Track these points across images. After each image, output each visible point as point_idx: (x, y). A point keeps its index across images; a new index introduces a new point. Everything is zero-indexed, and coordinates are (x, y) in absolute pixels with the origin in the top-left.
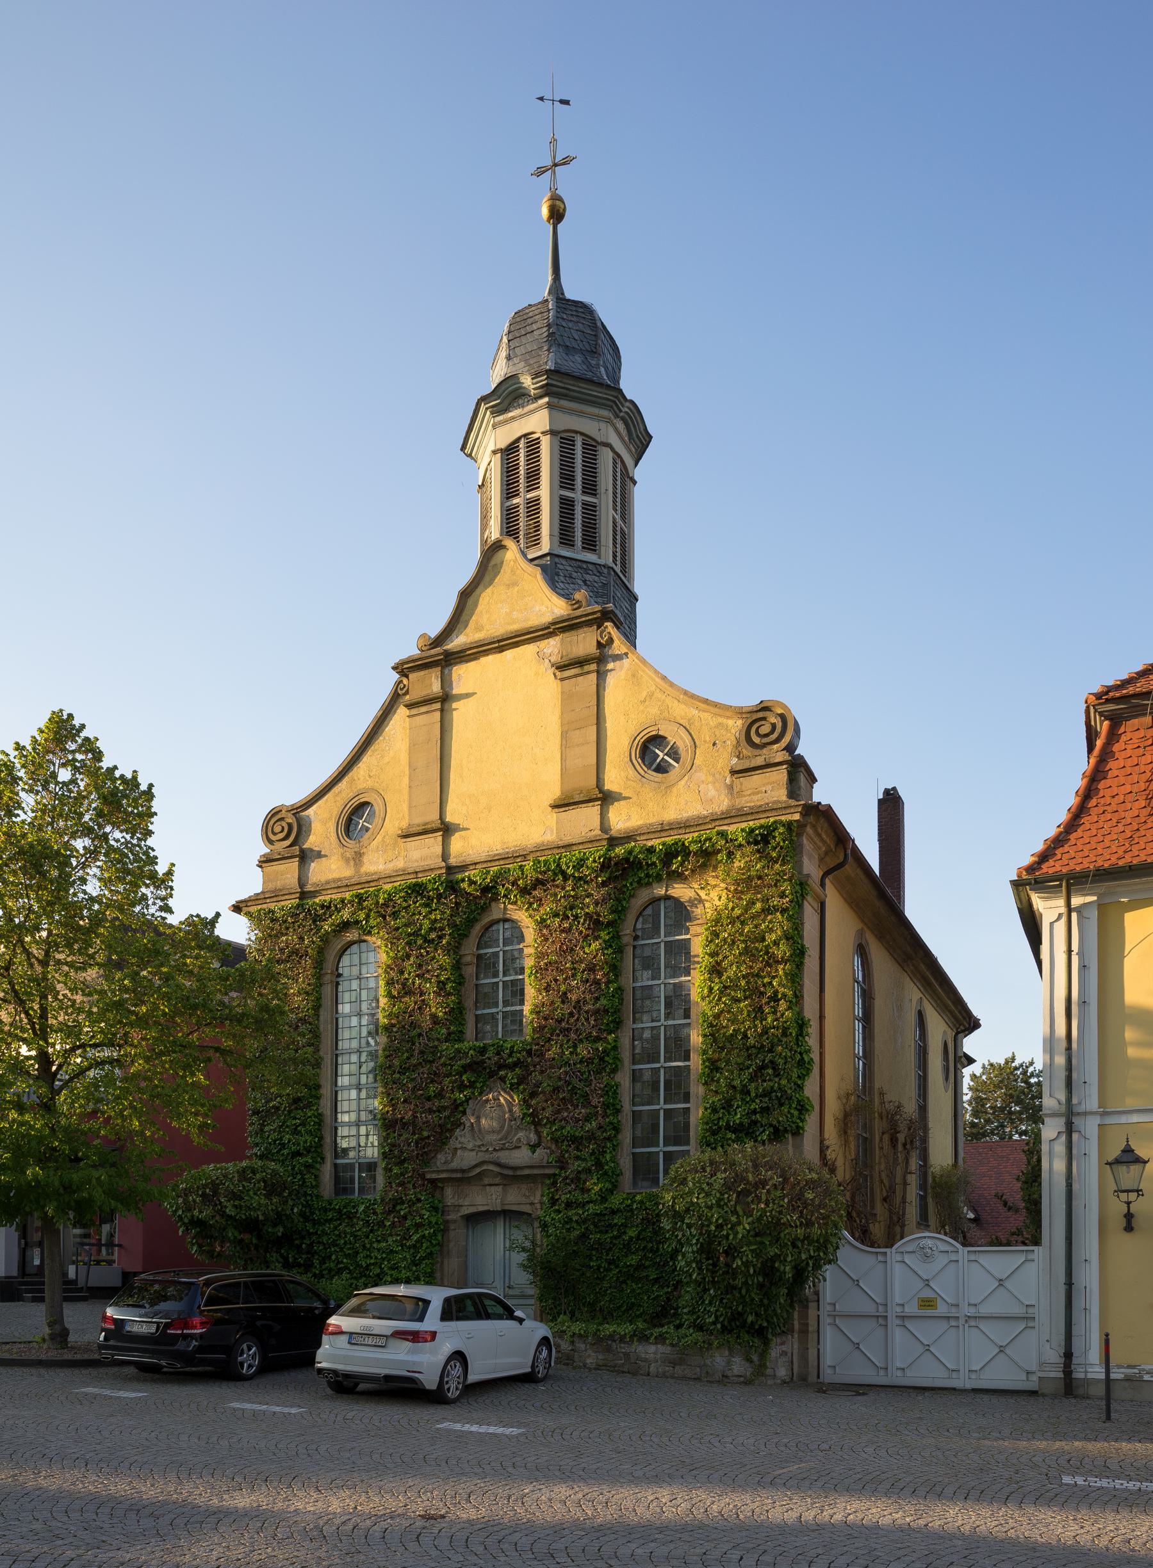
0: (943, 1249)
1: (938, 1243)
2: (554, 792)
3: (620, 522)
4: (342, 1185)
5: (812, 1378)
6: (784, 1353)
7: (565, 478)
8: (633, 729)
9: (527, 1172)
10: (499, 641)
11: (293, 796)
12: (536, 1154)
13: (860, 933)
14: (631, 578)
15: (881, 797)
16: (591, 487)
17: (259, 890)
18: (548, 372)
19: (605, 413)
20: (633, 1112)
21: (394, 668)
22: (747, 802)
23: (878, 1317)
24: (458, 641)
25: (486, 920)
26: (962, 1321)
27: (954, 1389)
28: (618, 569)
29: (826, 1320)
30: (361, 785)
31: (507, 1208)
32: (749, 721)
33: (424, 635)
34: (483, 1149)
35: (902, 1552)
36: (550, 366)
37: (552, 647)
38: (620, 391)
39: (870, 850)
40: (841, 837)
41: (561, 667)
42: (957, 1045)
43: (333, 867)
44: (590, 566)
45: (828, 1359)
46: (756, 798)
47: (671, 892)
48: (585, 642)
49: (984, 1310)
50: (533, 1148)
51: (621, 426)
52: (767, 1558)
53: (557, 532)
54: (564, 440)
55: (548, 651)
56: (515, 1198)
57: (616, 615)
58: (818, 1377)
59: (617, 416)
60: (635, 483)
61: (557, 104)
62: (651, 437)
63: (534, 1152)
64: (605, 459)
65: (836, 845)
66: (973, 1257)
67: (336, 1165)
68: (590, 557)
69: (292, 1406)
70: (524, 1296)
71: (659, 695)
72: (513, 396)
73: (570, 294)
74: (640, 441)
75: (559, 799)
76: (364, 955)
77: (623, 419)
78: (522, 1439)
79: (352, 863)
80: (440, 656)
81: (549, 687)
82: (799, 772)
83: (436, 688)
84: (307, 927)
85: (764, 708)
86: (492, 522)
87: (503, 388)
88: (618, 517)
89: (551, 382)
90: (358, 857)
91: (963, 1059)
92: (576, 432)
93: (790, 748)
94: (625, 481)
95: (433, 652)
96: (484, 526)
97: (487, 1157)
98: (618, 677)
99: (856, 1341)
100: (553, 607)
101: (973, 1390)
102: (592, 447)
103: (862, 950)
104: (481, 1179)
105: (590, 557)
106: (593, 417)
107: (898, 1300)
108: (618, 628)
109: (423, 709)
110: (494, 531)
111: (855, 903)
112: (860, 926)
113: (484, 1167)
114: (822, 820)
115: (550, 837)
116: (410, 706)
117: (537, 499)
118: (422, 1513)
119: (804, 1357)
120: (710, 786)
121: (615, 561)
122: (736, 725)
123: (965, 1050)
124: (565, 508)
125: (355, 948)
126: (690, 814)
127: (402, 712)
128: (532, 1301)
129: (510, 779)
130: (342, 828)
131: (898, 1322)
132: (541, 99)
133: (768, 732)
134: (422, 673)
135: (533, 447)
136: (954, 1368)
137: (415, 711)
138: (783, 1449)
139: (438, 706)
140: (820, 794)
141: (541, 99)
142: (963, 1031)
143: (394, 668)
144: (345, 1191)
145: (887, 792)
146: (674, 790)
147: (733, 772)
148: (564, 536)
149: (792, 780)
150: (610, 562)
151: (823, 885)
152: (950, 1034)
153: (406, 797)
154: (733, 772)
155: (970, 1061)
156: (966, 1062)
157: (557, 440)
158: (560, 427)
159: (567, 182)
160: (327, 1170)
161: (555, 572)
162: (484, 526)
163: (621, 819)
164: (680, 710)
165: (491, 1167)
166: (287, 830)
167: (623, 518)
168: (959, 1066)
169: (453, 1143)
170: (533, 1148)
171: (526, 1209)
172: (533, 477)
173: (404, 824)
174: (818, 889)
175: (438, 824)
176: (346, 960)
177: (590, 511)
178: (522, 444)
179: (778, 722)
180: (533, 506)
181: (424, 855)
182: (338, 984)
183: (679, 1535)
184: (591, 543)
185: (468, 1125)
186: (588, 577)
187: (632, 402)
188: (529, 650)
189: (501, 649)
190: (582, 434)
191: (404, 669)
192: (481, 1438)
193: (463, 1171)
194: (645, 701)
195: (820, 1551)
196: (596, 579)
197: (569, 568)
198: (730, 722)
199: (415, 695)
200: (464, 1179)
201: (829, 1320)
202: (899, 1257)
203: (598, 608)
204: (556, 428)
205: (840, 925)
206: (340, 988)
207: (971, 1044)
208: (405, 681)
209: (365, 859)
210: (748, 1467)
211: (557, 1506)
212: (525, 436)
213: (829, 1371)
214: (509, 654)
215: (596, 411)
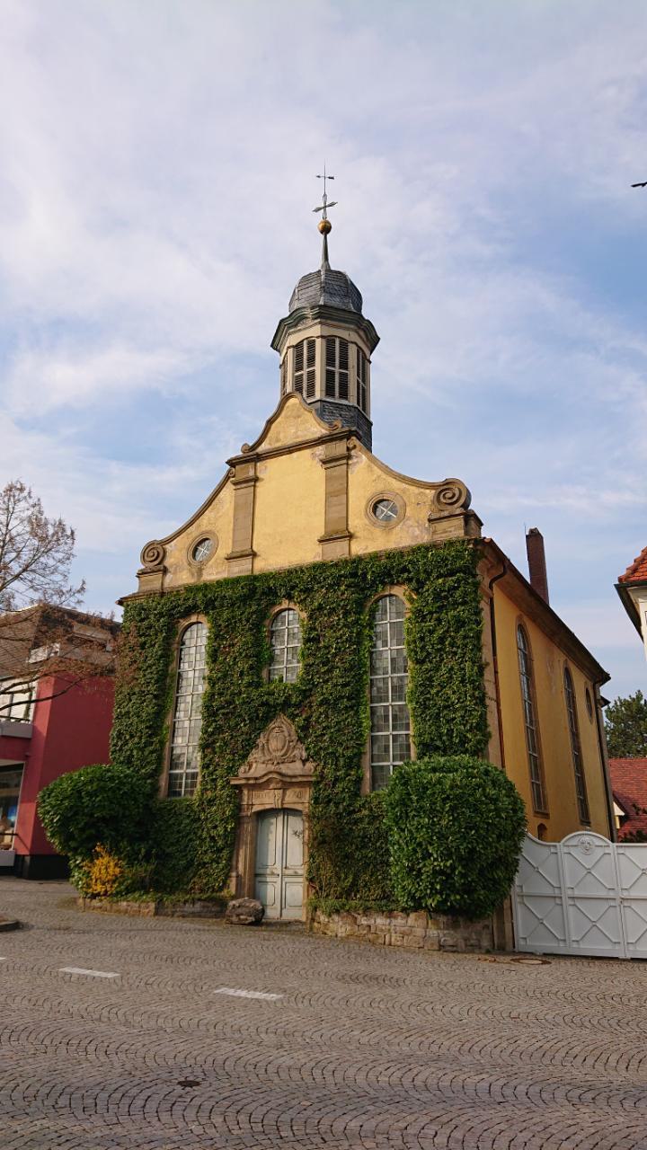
0: (597, 844)
1: (594, 839)
2: (321, 532)
3: (361, 383)
4: (173, 790)
5: (509, 947)
6: (487, 927)
7: (330, 360)
8: (368, 494)
9: (300, 779)
12: (306, 767)
13: (519, 618)
14: (369, 414)
15: (527, 534)
16: (344, 365)
17: (136, 591)
18: (320, 306)
20: (372, 736)
21: (227, 463)
22: (441, 537)
23: (555, 897)
24: (260, 449)
25: (277, 609)
26: (618, 902)
27: (617, 958)
28: (360, 408)
29: (516, 900)
30: (204, 529)
31: (285, 806)
35: (573, 1129)
36: (321, 303)
38: (362, 316)
39: (523, 568)
40: (501, 559)
41: (324, 462)
42: (596, 691)
43: (184, 577)
45: (521, 932)
46: (443, 535)
47: (392, 592)
48: (339, 448)
49: (633, 894)
50: (304, 762)
51: (362, 333)
52: (458, 1135)
53: (324, 389)
54: (329, 341)
55: (318, 453)
56: (291, 798)
57: (358, 433)
58: (514, 947)
59: (359, 328)
60: (370, 362)
62: (379, 339)
63: (304, 765)
64: (352, 351)
65: (498, 563)
66: (621, 851)
67: (170, 775)
68: (344, 402)
69: (109, 971)
70: (296, 875)
71: (384, 476)
73: (332, 268)
74: (373, 340)
76: (199, 632)
77: (363, 329)
78: (279, 1005)
80: (252, 456)
81: (320, 472)
82: (471, 519)
83: (251, 473)
84: (158, 617)
85: (448, 484)
86: (288, 384)
88: (360, 381)
90: (200, 571)
91: (601, 701)
92: (336, 336)
93: (465, 505)
94: (364, 362)
95: (251, 453)
96: (284, 385)
97: (273, 768)
98: (360, 461)
99: (587, 867)
100: (317, 429)
101: (632, 959)
103: (521, 629)
104: (269, 785)
105: (344, 402)
106: (345, 329)
107: (568, 885)
108: (359, 440)
109: (243, 485)
110: (289, 389)
111: (512, 597)
112: (518, 613)
113: (271, 776)
114: (487, 547)
115: (318, 559)
116: (235, 484)
117: (314, 371)
118: (183, 1079)
119: (502, 931)
120: (416, 529)
121: (358, 403)
122: (431, 493)
123: (602, 694)
124: (330, 376)
125: (195, 627)
126: (403, 545)
127: (229, 487)
128: (301, 880)
129: (291, 526)
131: (571, 902)
133: (452, 498)
135: (312, 344)
136: (617, 941)
138: (481, 1016)
139: (253, 483)
140: (486, 533)
142: (599, 682)
143: (227, 463)
145: (532, 531)
146: (394, 531)
148: (329, 390)
149: (466, 523)
150: (356, 405)
151: (491, 587)
152: (590, 684)
153: (231, 535)
154: (430, 520)
155: (607, 702)
156: (603, 703)
157: (324, 341)
158: (325, 334)
159: (332, 216)
160: (163, 783)
161: (323, 411)
162: (284, 385)
163: (359, 548)
164: (396, 484)
165: (275, 776)
166: (155, 555)
167: (364, 381)
168: (599, 706)
169: (251, 758)
170: (304, 762)
171: (299, 807)
172: (311, 360)
173: (229, 551)
174: (488, 591)
175: (249, 551)
176: (188, 634)
177: (344, 377)
178: (305, 342)
179: (457, 493)
180: (311, 375)
181: (240, 569)
182: (181, 650)
183: (387, 1107)
184: (344, 394)
185: (260, 745)
187: (368, 321)
188: (307, 452)
189: (291, 452)
190: (339, 337)
191: (232, 463)
192: (247, 1003)
193: (256, 779)
195: (503, 1126)
198: (428, 491)
199: (240, 477)
200: (258, 785)
201: (518, 900)
202: (566, 850)
203: (347, 429)
204: (324, 334)
205: (504, 617)
206: (183, 653)
207: (606, 691)
208: (233, 469)
209: (204, 572)
210: (453, 1034)
211: (295, 1074)
213: (522, 942)
214: (295, 455)
215: (347, 325)
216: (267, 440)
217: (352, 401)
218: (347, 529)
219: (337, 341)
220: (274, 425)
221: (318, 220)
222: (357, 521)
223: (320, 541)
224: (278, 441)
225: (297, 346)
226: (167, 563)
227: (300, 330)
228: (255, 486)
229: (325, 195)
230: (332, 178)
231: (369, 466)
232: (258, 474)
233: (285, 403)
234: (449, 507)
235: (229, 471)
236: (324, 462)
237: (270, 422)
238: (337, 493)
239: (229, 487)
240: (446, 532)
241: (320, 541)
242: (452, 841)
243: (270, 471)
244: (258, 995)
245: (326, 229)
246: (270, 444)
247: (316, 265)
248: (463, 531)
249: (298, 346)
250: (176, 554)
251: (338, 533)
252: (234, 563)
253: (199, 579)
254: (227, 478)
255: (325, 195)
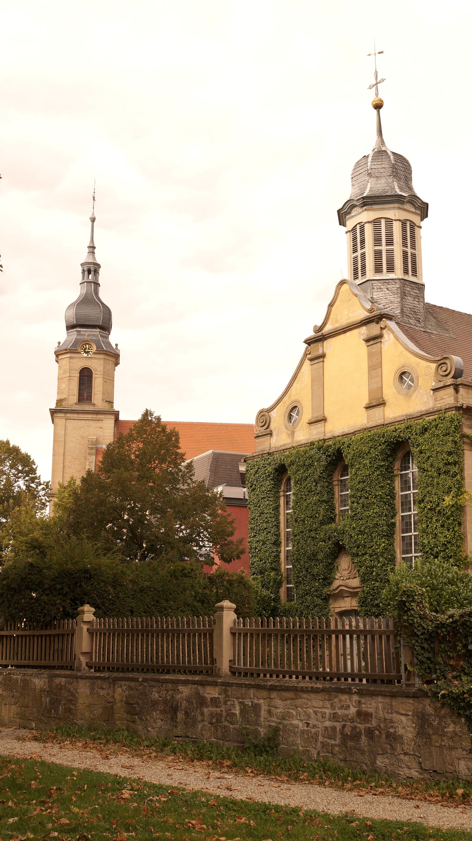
2: (365, 401)
7: (377, 241)
10: (343, 329)
11: (267, 406)
16: (390, 242)
19: (396, 205)
20: (287, 587)
22: (441, 404)
24: (328, 328)
30: (293, 398)
32: (438, 365)
33: (315, 326)
34: (342, 578)
37: (363, 330)
44: (390, 281)
46: (441, 401)
48: (374, 329)
61: (377, 55)
64: (397, 227)
68: (391, 276)
72: (352, 206)
75: (369, 404)
79: (291, 436)
80: (318, 339)
81: (363, 347)
83: (320, 352)
87: (346, 205)
89: (364, 201)
92: (382, 218)
102: (389, 221)
116: (311, 360)
121: (406, 271)
124: (378, 254)
130: (286, 418)
132: (370, 55)
134: (315, 344)
137: (313, 362)
141: (370, 55)
144: (291, 600)
147: (435, 390)
148: (378, 269)
172: (363, 242)
173: (310, 417)
177: (390, 254)
184: (391, 269)
186: (389, 286)
194: (399, 356)
196: (394, 286)
197: (380, 284)
212: (359, 224)
214: (348, 334)
215: (392, 206)
216: (330, 321)
217: (398, 273)
218: (382, 398)
219: (383, 221)
220: (334, 308)
221: (371, 98)
222: (390, 390)
223: (367, 408)
224: (337, 322)
225: (352, 230)
226: (272, 427)
227: (353, 216)
228: (323, 361)
229: (376, 72)
230: (382, 52)
231: (395, 343)
232: (325, 351)
233: (340, 289)
234: (445, 378)
235: (307, 348)
236: (367, 341)
237: (331, 305)
238: (375, 366)
239: (307, 363)
240: (443, 399)
241: (367, 408)
242: (170, 566)
243: (331, 347)
244: (203, 656)
245: (378, 106)
246: (332, 325)
247: (368, 147)
248: (453, 398)
249: (354, 229)
250: (278, 418)
251: (377, 403)
252: (313, 426)
253: (293, 440)
254: (305, 354)
255: (376, 72)
